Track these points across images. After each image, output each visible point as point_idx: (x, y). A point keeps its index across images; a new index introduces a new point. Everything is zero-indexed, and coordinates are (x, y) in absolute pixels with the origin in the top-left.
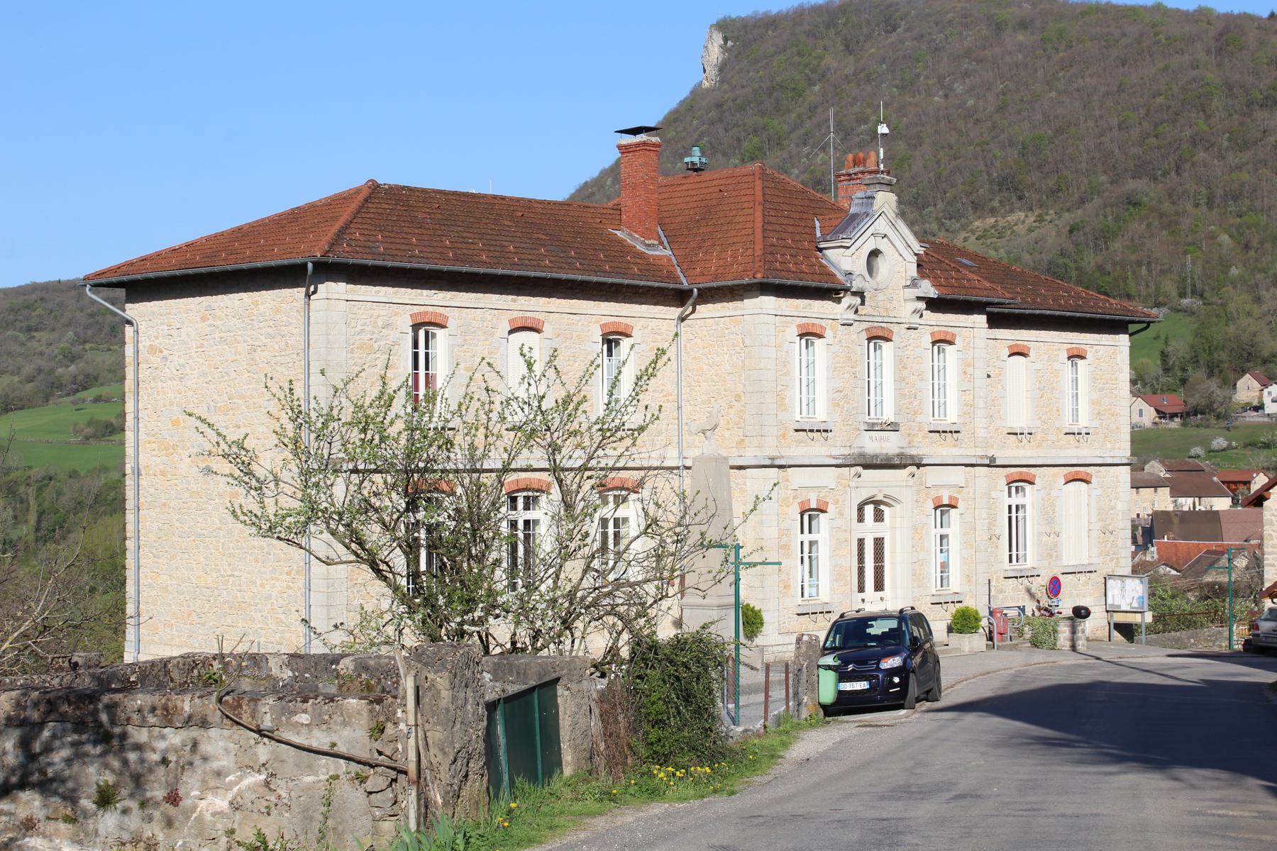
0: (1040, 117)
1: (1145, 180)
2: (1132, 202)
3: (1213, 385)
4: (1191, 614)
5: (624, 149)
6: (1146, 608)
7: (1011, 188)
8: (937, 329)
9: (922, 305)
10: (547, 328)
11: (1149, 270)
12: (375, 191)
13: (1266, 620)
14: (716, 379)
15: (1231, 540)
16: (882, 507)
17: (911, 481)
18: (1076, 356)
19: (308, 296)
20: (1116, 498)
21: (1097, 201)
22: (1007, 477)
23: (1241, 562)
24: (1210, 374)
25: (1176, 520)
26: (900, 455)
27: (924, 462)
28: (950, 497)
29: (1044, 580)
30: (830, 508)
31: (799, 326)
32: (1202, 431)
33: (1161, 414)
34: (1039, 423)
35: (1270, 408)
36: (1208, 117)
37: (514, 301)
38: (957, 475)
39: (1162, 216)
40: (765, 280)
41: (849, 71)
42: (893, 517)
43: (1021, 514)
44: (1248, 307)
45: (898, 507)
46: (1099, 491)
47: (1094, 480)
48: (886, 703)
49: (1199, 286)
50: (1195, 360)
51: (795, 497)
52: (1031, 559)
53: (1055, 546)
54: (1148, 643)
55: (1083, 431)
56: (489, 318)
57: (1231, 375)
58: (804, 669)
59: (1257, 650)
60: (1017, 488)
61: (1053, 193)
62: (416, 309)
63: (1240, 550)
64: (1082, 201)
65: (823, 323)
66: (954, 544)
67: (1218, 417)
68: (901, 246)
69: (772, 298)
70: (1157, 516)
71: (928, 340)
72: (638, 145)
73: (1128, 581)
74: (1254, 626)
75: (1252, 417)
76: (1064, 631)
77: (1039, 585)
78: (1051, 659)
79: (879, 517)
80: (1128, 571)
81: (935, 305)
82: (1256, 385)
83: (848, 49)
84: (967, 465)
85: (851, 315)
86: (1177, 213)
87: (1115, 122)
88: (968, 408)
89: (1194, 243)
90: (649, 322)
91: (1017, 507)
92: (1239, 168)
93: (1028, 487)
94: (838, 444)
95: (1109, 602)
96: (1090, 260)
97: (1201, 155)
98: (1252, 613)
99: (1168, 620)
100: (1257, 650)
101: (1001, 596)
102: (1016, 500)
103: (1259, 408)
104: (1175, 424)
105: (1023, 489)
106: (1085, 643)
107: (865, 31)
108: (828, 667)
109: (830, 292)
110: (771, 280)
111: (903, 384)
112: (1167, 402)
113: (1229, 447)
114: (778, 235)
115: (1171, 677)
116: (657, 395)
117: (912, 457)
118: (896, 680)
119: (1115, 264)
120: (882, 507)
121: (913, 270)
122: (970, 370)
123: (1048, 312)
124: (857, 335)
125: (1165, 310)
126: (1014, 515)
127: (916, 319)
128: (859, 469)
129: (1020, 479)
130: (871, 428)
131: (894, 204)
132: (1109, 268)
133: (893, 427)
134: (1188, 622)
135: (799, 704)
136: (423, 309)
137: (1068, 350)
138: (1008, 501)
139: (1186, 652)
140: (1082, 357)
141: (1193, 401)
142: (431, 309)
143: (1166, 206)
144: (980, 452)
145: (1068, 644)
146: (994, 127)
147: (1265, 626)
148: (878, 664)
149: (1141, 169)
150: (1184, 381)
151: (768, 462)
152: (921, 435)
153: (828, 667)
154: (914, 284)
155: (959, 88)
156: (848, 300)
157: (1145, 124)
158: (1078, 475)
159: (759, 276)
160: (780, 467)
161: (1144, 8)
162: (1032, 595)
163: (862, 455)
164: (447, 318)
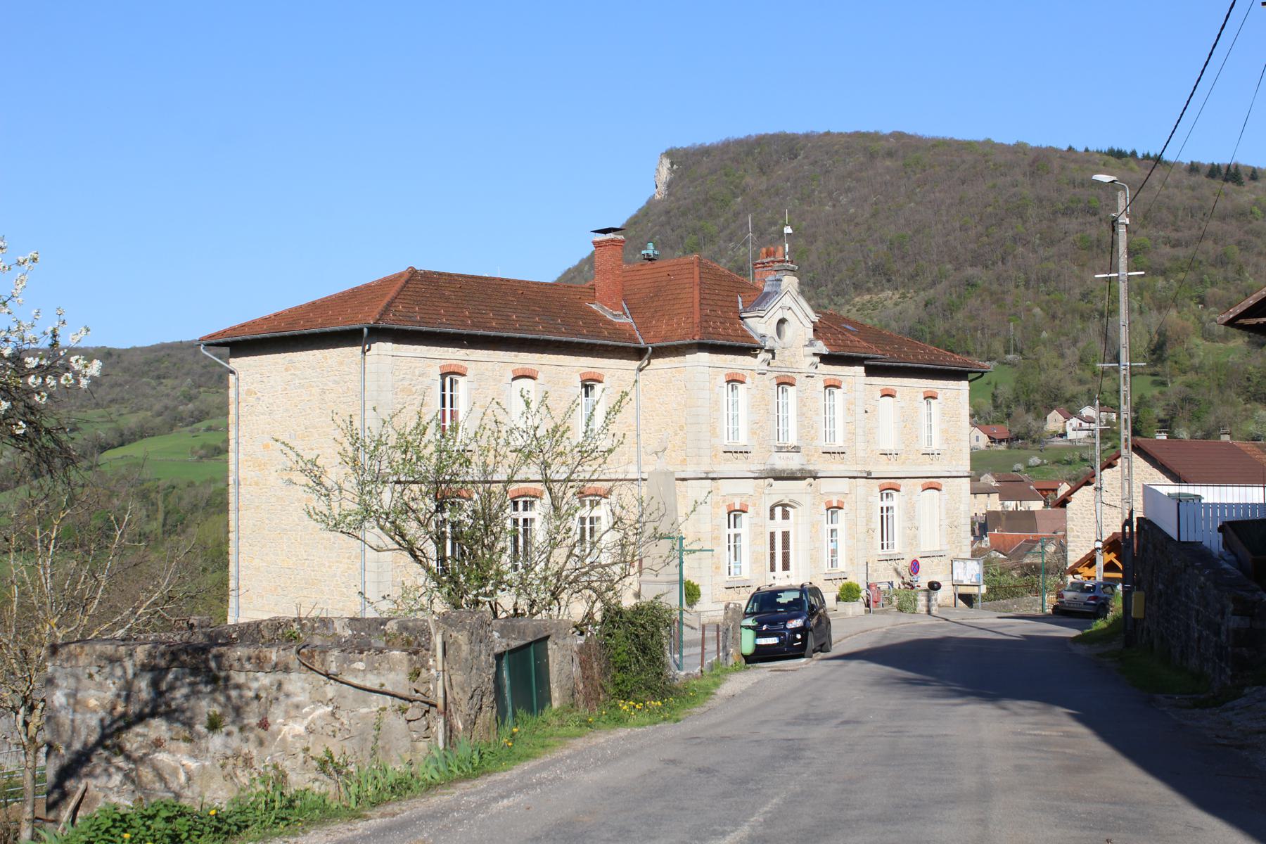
0: (902, 221)
2: (971, 284)
3: (1030, 418)
5: (598, 244)
7: (882, 274)
9: (817, 359)
11: (983, 334)
17: (810, 490)
19: (364, 352)
21: (944, 283)
23: (1051, 548)
24: (1028, 411)
25: (1003, 518)
26: (801, 470)
29: (907, 562)
30: (750, 510)
32: (1022, 452)
35: (1071, 435)
36: (1025, 222)
39: (992, 294)
41: (763, 187)
43: (890, 513)
44: (1055, 361)
49: (1019, 345)
50: (1017, 400)
52: (898, 547)
54: (983, 608)
61: (913, 277)
63: (1050, 539)
64: (934, 283)
65: (744, 372)
66: (841, 536)
67: (1034, 442)
68: (801, 316)
72: (607, 241)
73: (969, 563)
74: (1060, 595)
75: (1059, 442)
76: (922, 600)
77: (904, 566)
79: (786, 516)
80: (968, 555)
81: (826, 359)
82: (1061, 418)
85: (765, 367)
86: (1003, 292)
92: (1047, 259)
96: (940, 326)
97: (1020, 249)
98: (1058, 586)
99: (997, 591)
102: (886, 503)
103: (1064, 435)
104: (1003, 447)
107: (775, 157)
108: (749, 627)
109: (748, 349)
110: (706, 341)
113: (1042, 464)
117: (810, 471)
118: (799, 636)
119: (958, 329)
121: (810, 334)
122: (852, 407)
124: (770, 382)
125: (995, 363)
127: (812, 369)
129: (890, 487)
130: (780, 450)
132: (954, 332)
133: (797, 450)
134: (1012, 592)
140: (934, 398)
141: (1015, 430)
144: (860, 468)
145: (925, 609)
146: (869, 228)
149: (977, 260)
150: (1008, 415)
153: (749, 627)
154: (811, 344)
156: (763, 356)
157: (979, 228)
160: (713, 479)
161: (978, 142)
163: (773, 470)
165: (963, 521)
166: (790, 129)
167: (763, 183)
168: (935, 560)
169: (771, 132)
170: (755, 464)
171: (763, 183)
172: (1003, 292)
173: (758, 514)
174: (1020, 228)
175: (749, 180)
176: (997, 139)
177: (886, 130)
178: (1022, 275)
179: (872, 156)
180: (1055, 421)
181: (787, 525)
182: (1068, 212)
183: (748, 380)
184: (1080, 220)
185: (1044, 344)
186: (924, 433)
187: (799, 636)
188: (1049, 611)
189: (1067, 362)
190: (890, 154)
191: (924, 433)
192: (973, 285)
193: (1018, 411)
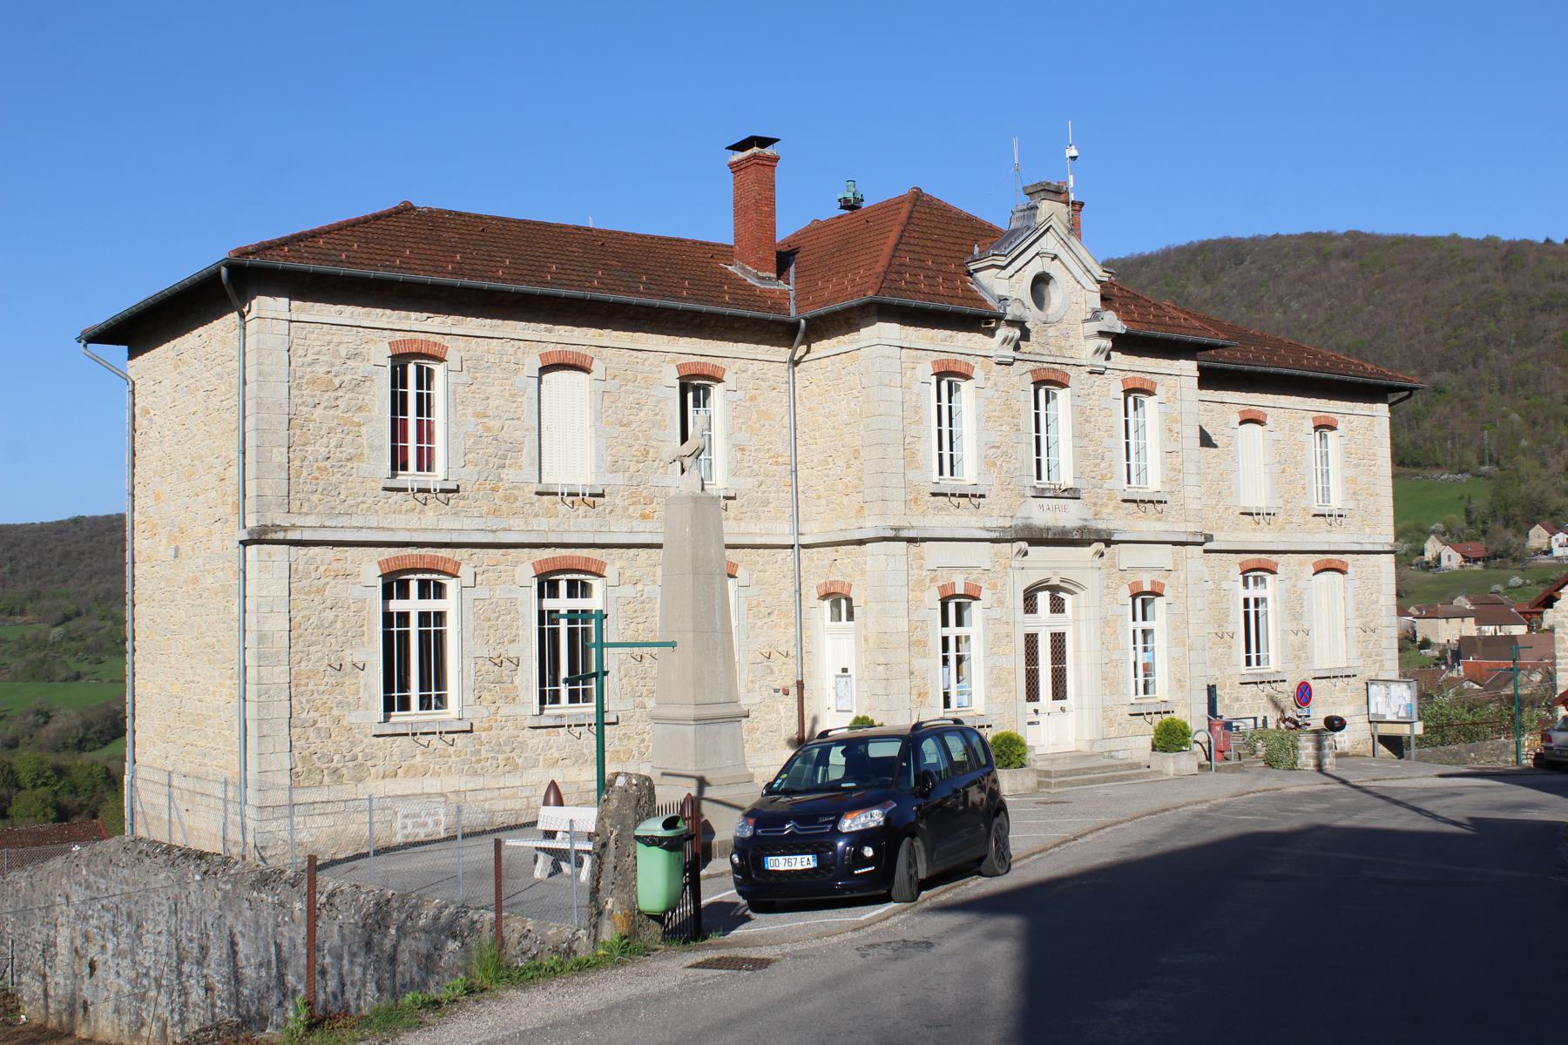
0: (1360, 325)
1: (1448, 372)
3: (1509, 534)
4: (1474, 723)
5: (736, 167)
6: (1415, 718)
8: (1130, 375)
9: (1107, 343)
10: (597, 366)
11: (1453, 444)
12: (406, 210)
13: (1560, 730)
14: (833, 432)
15: (1527, 659)
16: (1061, 595)
17: (1098, 562)
18: (1324, 427)
19: (242, 316)
20: (1379, 592)
22: (1241, 564)
23: (1537, 677)
24: (1507, 526)
25: (1480, 644)
26: (1081, 530)
28: (1153, 582)
29: (1290, 688)
30: (985, 594)
31: (934, 363)
32: (1502, 572)
33: (1466, 559)
34: (1280, 503)
35: (1558, 552)
36: (1497, 321)
37: (547, 330)
38: (1163, 556)
39: (1462, 400)
40: (879, 298)
41: (1207, 295)
42: (1076, 607)
43: (1261, 609)
44: (1536, 471)
45: (1082, 594)
46: (1357, 583)
48: (848, 895)
49: (1495, 455)
50: (1494, 515)
51: (932, 580)
52: (1274, 659)
53: (1304, 646)
54: (1419, 758)
55: (1336, 513)
56: (511, 351)
57: (1524, 526)
58: (612, 845)
59: (1559, 769)
60: (1255, 578)
62: (398, 336)
63: (1534, 669)
65: (971, 360)
66: (1160, 641)
67: (1514, 560)
69: (896, 326)
70: (1464, 640)
71: (1117, 389)
72: (748, 159)
73: (1393, 686)
74: (1546, 738)
75: (1543, 560)
76: (1307, 748)
78: (1278, 784)
79: (1057, 606)
80: (1395, 675)
81: (1124, 343)
82: (1545, 533)
83: (1207, 280)
84: (1175, 543)
85: (1009, 352)
86: (1475, 398)
87: (1422, 328)
88: (1174, 474)
89: (1489, 421)
90: (744, 364)
91: (1256, 601)
92: (1525, 360)
93: (1269, 577)
94: (996, 513)
95: (1372, 711)
97: (1494, 351)
98: (1546, 722)
99: (1445, 729)
100: (1559, 769)
101: (1236, 706)
102: (1253, 593)
103: (1549, 551)
104: (1479, 566)
105: (1263, 580)
106: (1334, 761)
107: (1219, 264)
108: (651, 841)
109: (978, 320)
110: (887, 298)
111: (1085, 442)
112: (1470, 548)
113: (1524, 584)
114: (913, 256)
115: (1435, 817)
116: (761, 455)
117: (1098, 531)
118: (869, 852)
119: (1425, 440)
120: (1061, 595)
121: (1096, 302)
122: (1176, 427)
123: (1286, 371)
124: (1020, 381)
125: (1467, 476)
126: (1252, 609)
127: (1100, 361)
128: (1024, 545)
129: (1258, 567)
130: (1040, 494)
131: (1065, 218)
132: (1420, 443)
133: (1073, 494)
134: (1470, 734)
135: (600, 914)
136: (409, 336)
138: (1243, 593)
139: (1463, 770)
140: (1332, 428)
141: (1492, 548)
142: (422, 336)
143: (1466, 392)
144: (1192, 528)
145: (1312, 762)
146: (1324, 334)
147: (1560, 738)
148: (836, 822)
149: (1444, 364)
150: (1484, 532)
151: (891, 534)
152: (1111, 504)
153: (651, 841)
154: (1096, 316)
155: (1295, 305)
156: (1003, 332)
157: (1446, 329)
158: (1331, 563)
159: (870, 293)
160: (911, 540)
161: (1443, 238)
162: (1276, 704)
163: (1029, 528)
166: (1235, 233)
167: (1207, 292)
168: (1339, 682)
169: (1214, 237)
170: (994, 517)
171: (1207, 292)
172: (1475, 398)
173: (1000, 602)
174: (1492, 326)
175: (1192, 289)
176: (1464, 234)
177: (1341, 229)
178: (1496, 379)
179: (1326, 258)
180: (1538, 536)
181: (1059, 623)
182: (1547, 308)
183: (978, 373)
184: (1561, 316)
185: (1524, 453)
186: (1315, 485)
187: (869, 852)
188: (1528, 762)
189: (1550, 471)
190: (1345, 254)
191: (1315, 485)
192: (1442, 392)
193: (1495, 527)
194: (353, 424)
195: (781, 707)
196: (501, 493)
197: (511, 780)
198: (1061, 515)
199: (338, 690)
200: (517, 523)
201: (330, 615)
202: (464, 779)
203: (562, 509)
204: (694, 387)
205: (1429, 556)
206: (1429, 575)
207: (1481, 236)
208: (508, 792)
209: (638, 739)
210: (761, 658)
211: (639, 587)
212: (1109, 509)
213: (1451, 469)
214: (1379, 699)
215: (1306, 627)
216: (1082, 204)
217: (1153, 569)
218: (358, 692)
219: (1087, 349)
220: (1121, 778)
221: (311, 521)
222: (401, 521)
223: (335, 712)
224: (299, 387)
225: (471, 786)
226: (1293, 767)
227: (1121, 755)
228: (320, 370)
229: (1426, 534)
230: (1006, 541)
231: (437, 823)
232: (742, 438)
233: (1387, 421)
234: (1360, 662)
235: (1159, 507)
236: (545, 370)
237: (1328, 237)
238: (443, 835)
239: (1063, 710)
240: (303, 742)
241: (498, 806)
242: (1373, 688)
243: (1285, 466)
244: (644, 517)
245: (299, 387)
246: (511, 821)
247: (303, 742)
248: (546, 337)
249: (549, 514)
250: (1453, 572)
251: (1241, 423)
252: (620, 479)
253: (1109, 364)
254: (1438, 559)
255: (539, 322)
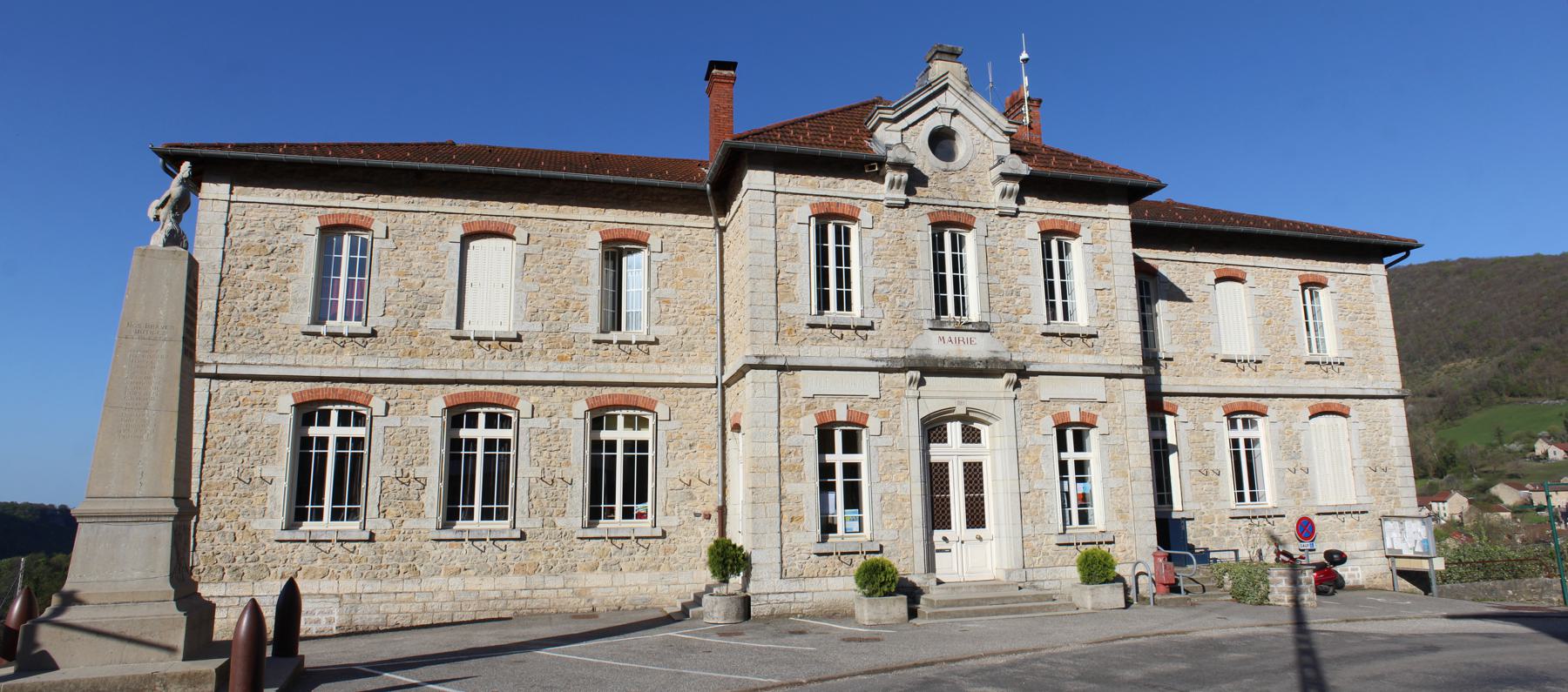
2: (1535, 349)
6: (1432, 553)
7: (1462, 349)
27: (1031, 368)
28: (1082, 414)
31: (812, 206)
42: (992, 436)
45: (996, 424)
46: (1362, 425)
47: (1352, 413)
51: (808, 408)
53: (1304, 484)
54: (1440, 595)
61: (1487, 348)
64: (1504, 351)
65: (857, 204)
66: (1094, 472)
68: (983, 125)
77: (1286, 529)
79: (971, 436)
81: (1032, 186)
93: (1260, 420)
95: (1388, 545)
96: (1513, 379)
101: (1227, 539)
109: (866, 167)
120: (976, 425)
122: (1106, 267)
128: (916, 374)
134: (1514, 570)
136: (339, 211)
137: (1300, 277)
149: (1538, 332)
151: (756, 361)
155: (1426, 304)
158: (1328, 406)
160: (781, 369)
162: (1275, 540)
164: (1095, 417)
165: (1398, 462)
176: (1545, 252)
177: (1455, 258)
179: (1445, 275)
190: (1459, 272)
194: (281, 281)
195: (702, 530)
196: (418, 338)
197: (409, 586)
198: (963, 347)
199: (246, 500)
200: (431, 363)
201: (244, 437)
202: (361, 582)
203: (478, 352)
204: (615, 252)
205: (1538, 452)
206: (1541, 464)
207: (1558, 253)
208: (404, 597)
209: (545, 555)
210: (680, 485)
211: (554, 419)
212: (1028, 342)
213: (1550, 397)
214: (1394, 535)
215: (1304, 465)
216: (1040, 101)
217: (1082, 400)
218: (264, 502)
219: (994, 194)
220: (1019, 611)
221: (232, 359)
222: (329, 360)
223: (241, 520)
224: (235, 252)
225: (368, 589)
226: (1263, 600)
227: (1046, 585)
228: (255, 239)
229: (1536, 438)
230: (899, 371)
231: (330, 621)
232: (667, 292)
233: (1385, 280)
234: (1373, 499)
235: (1089, 341)
236: (466, 239)
237: (1447, 263)
238: (335, 632)
239: (980, 539)
240: (208, 544)
241: (393, 609)
242: (1388, 525)
243: (1268, 319)
244: (562, 359)
245: (235, 252)
246: (406, 623)
247: (208, 544)
248: (469, 210)
249: (463, 355)
250: (1557, 462)
251: (1218, 280)
252: (537, 326)
253: (1022, 208)
254: (1546, 454)
255: (465, 198)
